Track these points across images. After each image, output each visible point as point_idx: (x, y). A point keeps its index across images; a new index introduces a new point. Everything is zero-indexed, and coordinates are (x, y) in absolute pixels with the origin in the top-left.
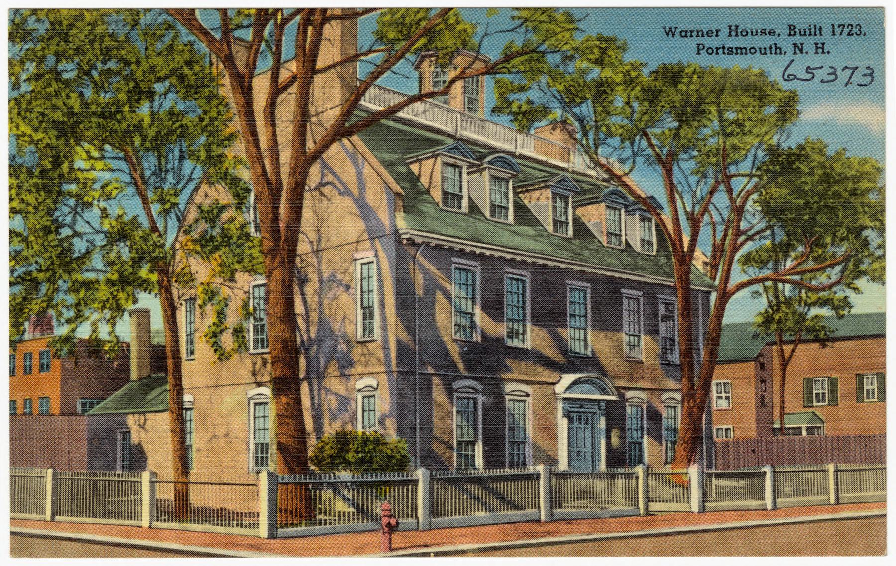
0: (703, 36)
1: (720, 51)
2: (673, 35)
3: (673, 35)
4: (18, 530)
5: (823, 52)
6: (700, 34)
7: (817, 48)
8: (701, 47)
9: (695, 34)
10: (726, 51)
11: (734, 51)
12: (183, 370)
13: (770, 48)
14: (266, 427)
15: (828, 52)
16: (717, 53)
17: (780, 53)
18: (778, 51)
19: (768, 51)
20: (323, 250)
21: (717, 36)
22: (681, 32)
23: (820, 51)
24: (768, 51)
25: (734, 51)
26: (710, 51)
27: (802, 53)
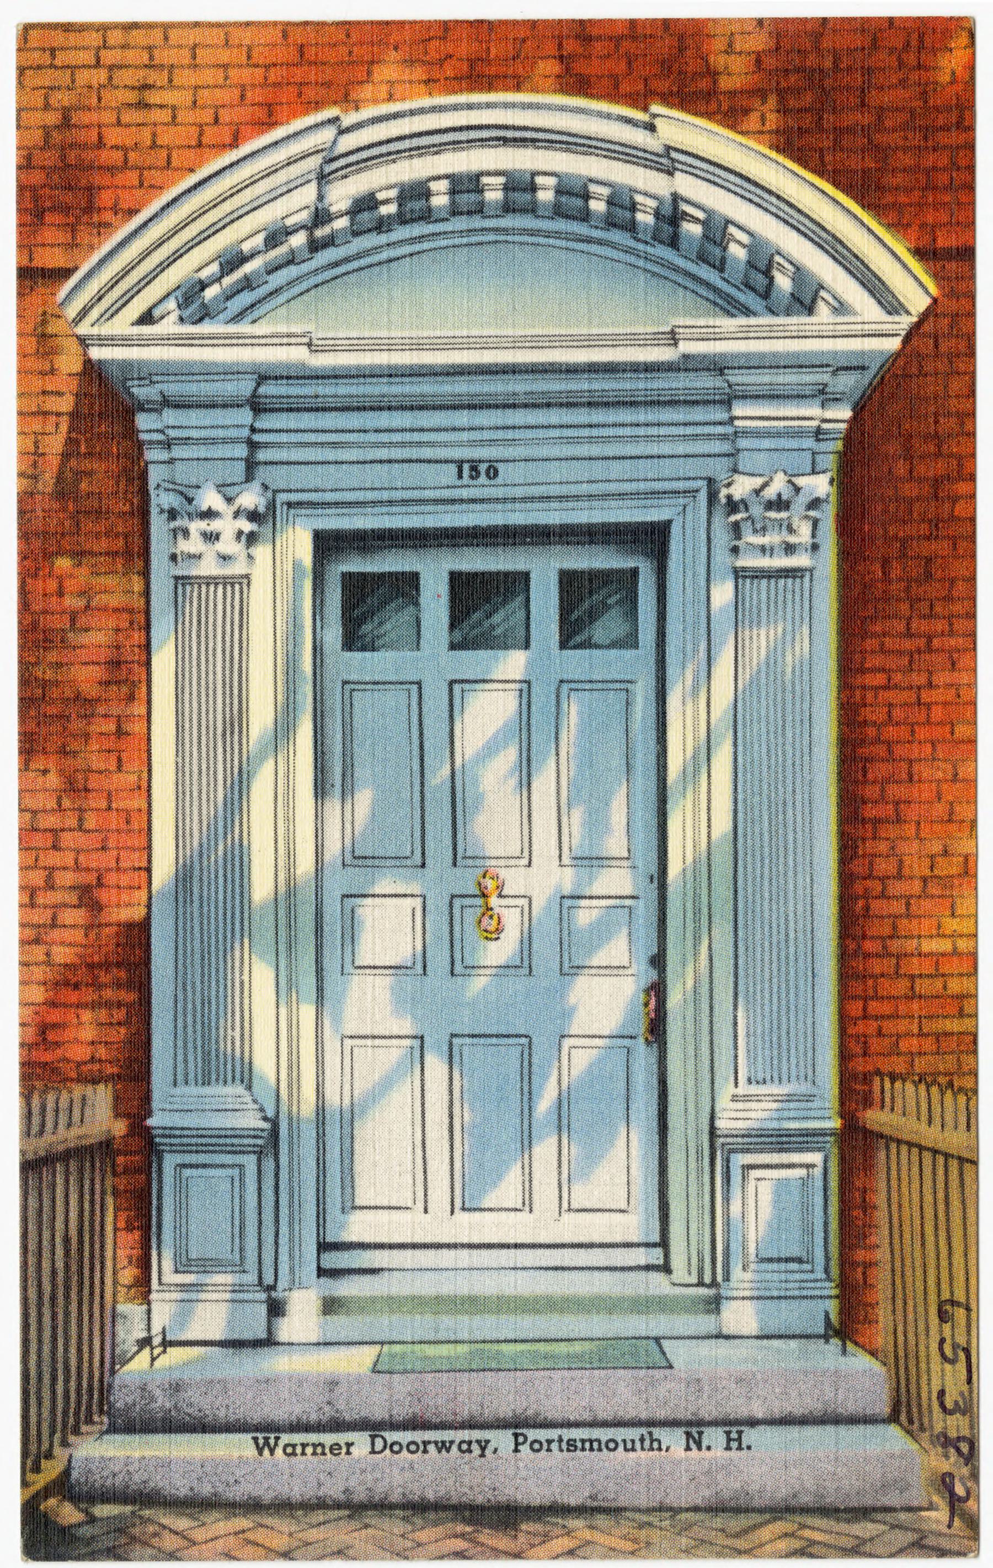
0: (324, 1454)
1: (554, 1446)
2: (272, 1452)
3: (272, 1452)
4: (214, 1077)
5: (740, 1448)
6: (319, 1450)
7: (729, 1440)
8: (521, 1439)
9: (309, 1450)
10: (564, 1446)
11: (579, 1445)
12: (153, 968)
13: (642, 1440)
14: (474, 890)
15: (749, 1448)
16: (549, 1450)
17: (660, 1449)
18: (655, 1445)
19: (638, 1445)
20: (133, 88)
21: (348, 1453)
22: (286, 1446)
23: (734, 1445)
24: (638, 1445)
25: (579, 1445)
26: (536, 1446)
27: (700, 1448)
